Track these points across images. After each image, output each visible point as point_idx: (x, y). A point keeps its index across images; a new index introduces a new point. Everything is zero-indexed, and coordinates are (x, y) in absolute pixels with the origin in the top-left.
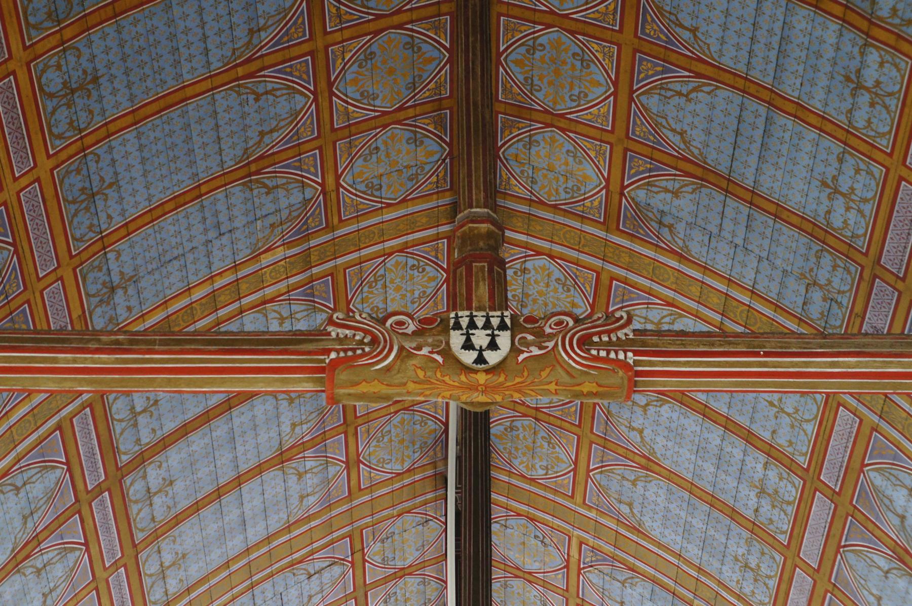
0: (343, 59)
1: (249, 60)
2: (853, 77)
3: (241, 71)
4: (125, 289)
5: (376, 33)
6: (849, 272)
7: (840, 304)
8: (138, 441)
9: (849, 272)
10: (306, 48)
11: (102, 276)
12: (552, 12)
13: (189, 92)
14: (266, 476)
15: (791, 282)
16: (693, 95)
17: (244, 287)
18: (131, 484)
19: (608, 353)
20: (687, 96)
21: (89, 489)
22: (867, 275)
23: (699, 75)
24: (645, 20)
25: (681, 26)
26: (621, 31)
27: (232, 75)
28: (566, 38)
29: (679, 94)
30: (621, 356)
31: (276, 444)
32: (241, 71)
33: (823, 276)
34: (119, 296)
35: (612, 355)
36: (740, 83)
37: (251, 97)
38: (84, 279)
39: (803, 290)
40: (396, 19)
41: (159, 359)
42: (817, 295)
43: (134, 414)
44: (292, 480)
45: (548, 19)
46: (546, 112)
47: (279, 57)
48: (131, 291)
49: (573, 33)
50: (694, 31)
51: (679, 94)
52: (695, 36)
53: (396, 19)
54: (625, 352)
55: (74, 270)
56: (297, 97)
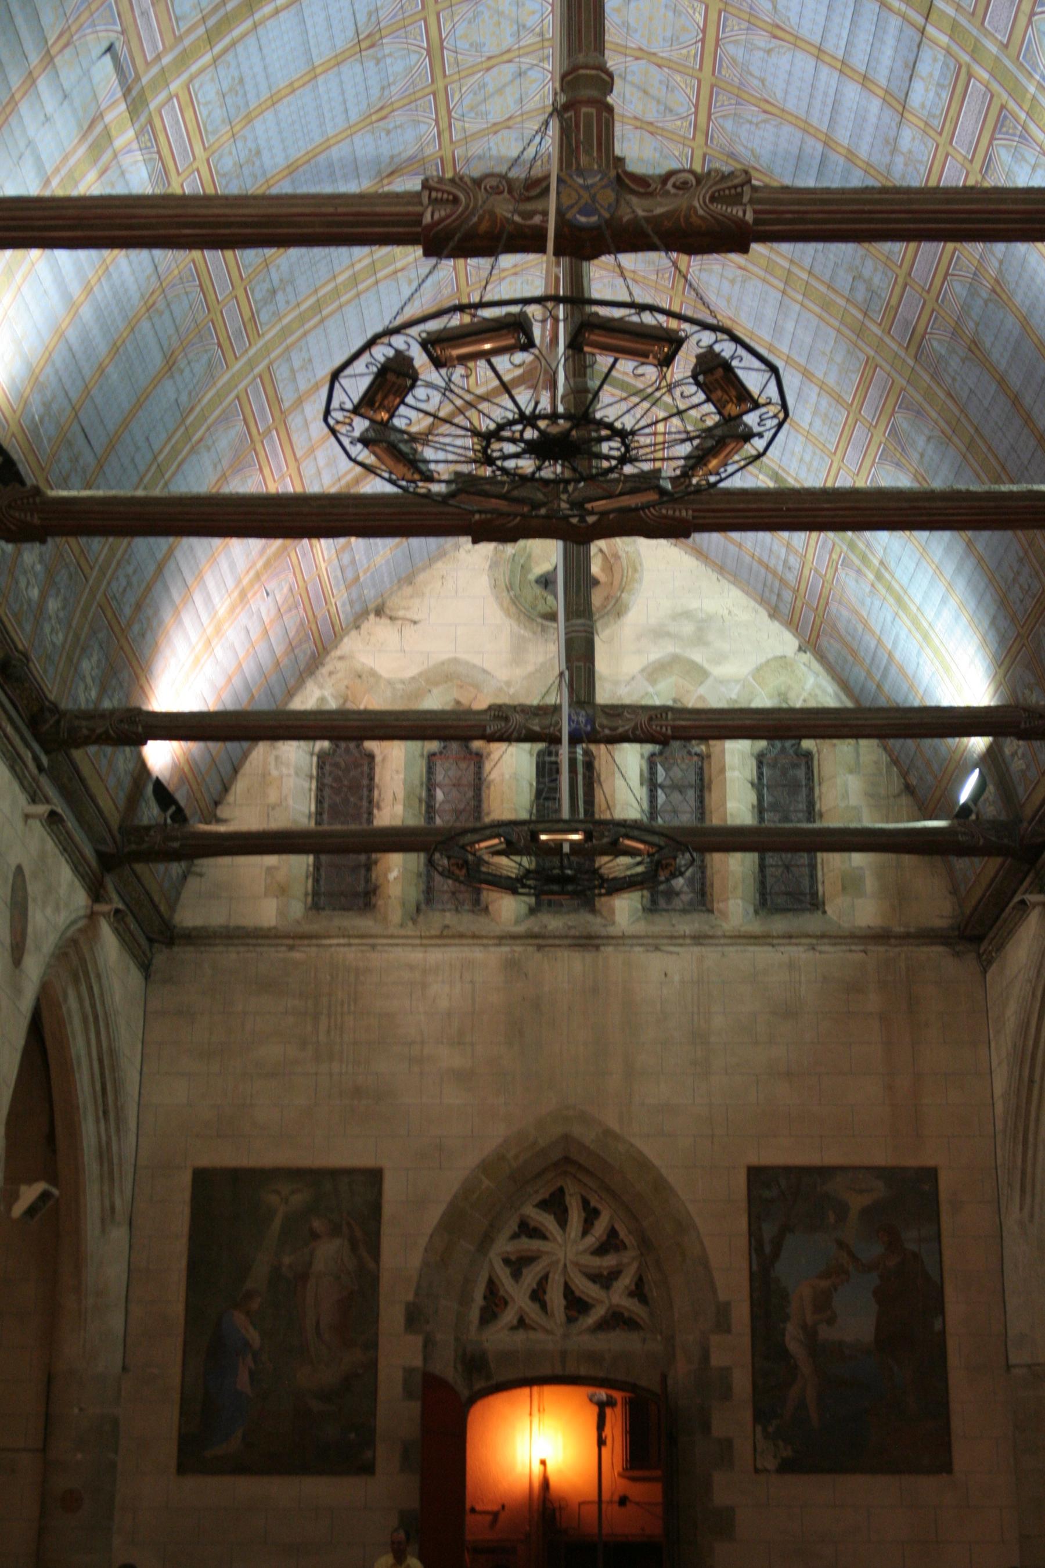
0: (453, 21)
1: (382, 108)
2: (891, 141)
3: (374, 118)
4: (284, 290)
5: (488, 69)
6: (886, 275)
7: (880, 297)
8: (297, 389)
9: (886, 275)
10: (428, 90)
11: (266, 286)
12: (641, 49)
13: (332, 142)
14: (345, 68)
15: (841, 273)
16: (762, 125)
17: (378, 266)
18: (278, 368)
19: (674, 511)
20: (757, 124)
21: (149, 59)
22: (900, 280)
23: (765, 112)
24: (721, 66)
25: (751, 74)
26: (694, 138)
27: (368, 121)
28: (653, 69)
29: (751, 123)
30: (684, 513)
31: (351, 33)
32: (374, 118)
33: (867, 273)
34: (280, 297)
35: (677, 513)
36: (802, 125)
37: (383, 134)
38: (253, 291)
39: (851, 280)
40: (506, 57)
41: (456, 941)
42: (861, 287)
43: (293, 371)
44: (370, 65)
45: (639, 54)
46: (636, 118)
47: (406, 101)
48: (289, 289)
49: (659, 66)
50: (763, 81)
51: (751, 123)
52: (763, 85)
53: (506, 57)
54: (687, 511)
55: (245, 289)
56: (421, 125)
